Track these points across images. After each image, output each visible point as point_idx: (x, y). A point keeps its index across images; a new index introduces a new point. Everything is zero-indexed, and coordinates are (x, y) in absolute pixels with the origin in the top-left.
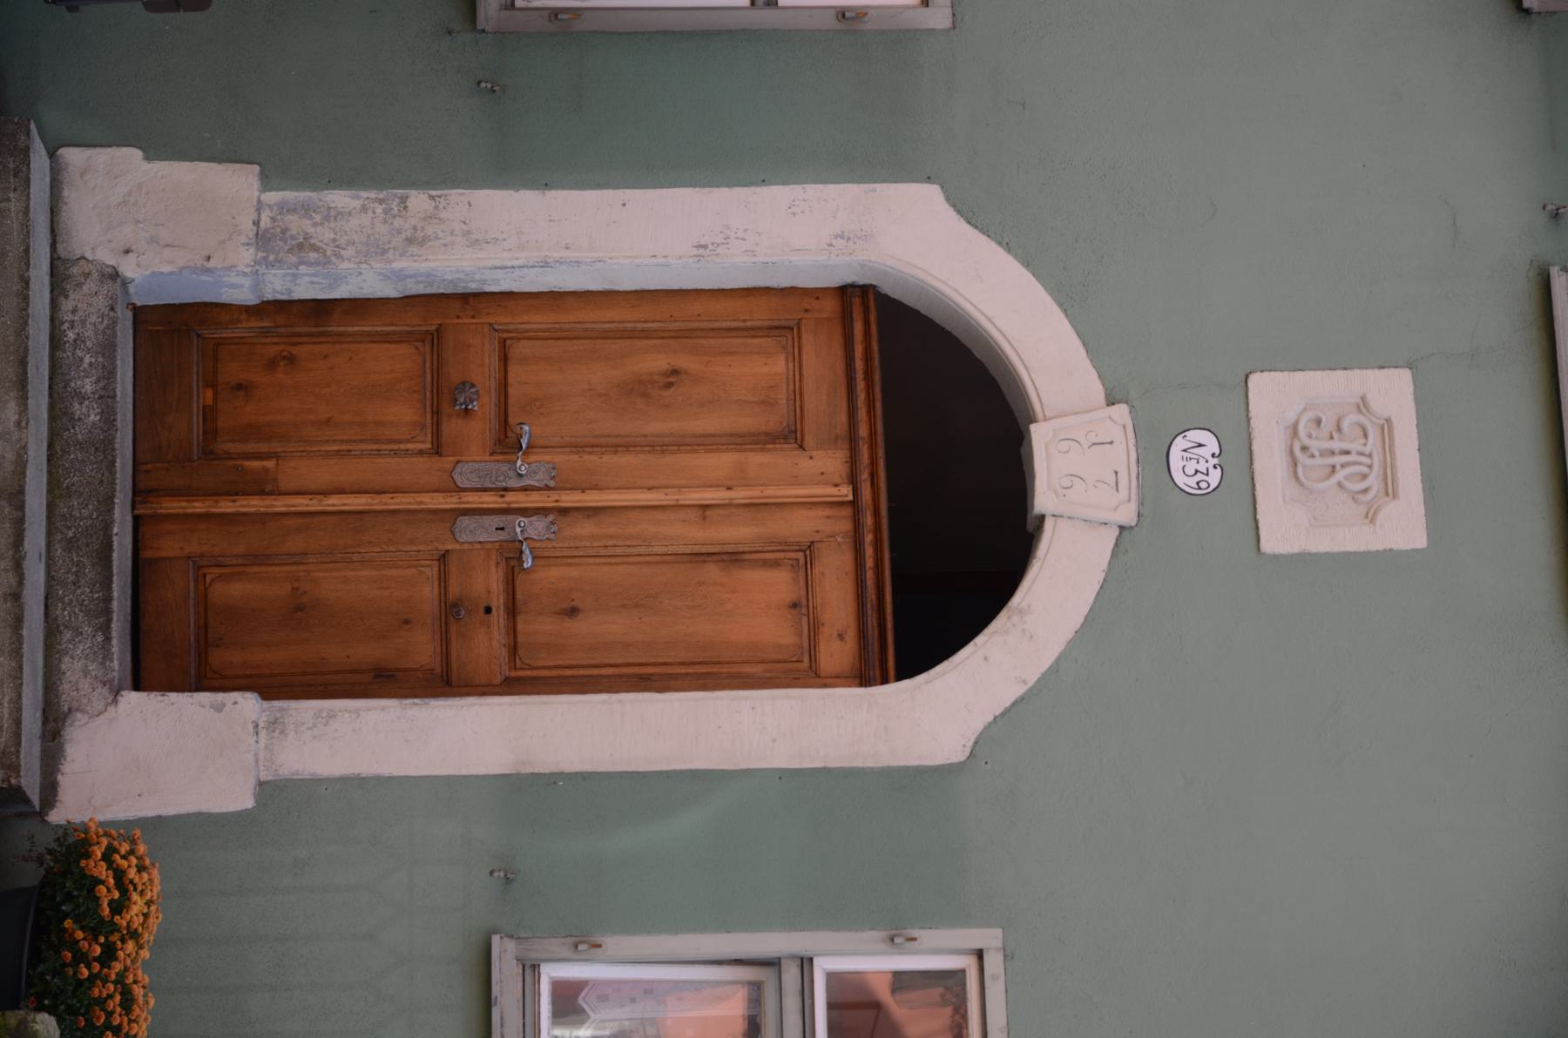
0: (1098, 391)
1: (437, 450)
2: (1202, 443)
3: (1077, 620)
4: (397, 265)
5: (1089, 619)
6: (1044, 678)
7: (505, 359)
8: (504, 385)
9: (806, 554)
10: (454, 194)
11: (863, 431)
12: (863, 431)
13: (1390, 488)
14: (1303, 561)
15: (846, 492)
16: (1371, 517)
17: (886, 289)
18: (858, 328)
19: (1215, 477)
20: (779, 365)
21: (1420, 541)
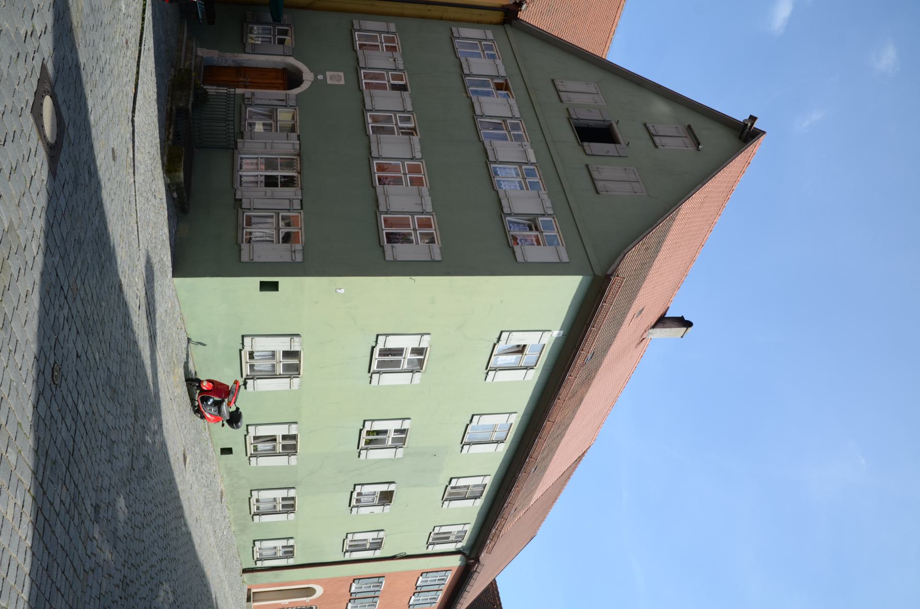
3: (307, 87)
13: (341, 80)
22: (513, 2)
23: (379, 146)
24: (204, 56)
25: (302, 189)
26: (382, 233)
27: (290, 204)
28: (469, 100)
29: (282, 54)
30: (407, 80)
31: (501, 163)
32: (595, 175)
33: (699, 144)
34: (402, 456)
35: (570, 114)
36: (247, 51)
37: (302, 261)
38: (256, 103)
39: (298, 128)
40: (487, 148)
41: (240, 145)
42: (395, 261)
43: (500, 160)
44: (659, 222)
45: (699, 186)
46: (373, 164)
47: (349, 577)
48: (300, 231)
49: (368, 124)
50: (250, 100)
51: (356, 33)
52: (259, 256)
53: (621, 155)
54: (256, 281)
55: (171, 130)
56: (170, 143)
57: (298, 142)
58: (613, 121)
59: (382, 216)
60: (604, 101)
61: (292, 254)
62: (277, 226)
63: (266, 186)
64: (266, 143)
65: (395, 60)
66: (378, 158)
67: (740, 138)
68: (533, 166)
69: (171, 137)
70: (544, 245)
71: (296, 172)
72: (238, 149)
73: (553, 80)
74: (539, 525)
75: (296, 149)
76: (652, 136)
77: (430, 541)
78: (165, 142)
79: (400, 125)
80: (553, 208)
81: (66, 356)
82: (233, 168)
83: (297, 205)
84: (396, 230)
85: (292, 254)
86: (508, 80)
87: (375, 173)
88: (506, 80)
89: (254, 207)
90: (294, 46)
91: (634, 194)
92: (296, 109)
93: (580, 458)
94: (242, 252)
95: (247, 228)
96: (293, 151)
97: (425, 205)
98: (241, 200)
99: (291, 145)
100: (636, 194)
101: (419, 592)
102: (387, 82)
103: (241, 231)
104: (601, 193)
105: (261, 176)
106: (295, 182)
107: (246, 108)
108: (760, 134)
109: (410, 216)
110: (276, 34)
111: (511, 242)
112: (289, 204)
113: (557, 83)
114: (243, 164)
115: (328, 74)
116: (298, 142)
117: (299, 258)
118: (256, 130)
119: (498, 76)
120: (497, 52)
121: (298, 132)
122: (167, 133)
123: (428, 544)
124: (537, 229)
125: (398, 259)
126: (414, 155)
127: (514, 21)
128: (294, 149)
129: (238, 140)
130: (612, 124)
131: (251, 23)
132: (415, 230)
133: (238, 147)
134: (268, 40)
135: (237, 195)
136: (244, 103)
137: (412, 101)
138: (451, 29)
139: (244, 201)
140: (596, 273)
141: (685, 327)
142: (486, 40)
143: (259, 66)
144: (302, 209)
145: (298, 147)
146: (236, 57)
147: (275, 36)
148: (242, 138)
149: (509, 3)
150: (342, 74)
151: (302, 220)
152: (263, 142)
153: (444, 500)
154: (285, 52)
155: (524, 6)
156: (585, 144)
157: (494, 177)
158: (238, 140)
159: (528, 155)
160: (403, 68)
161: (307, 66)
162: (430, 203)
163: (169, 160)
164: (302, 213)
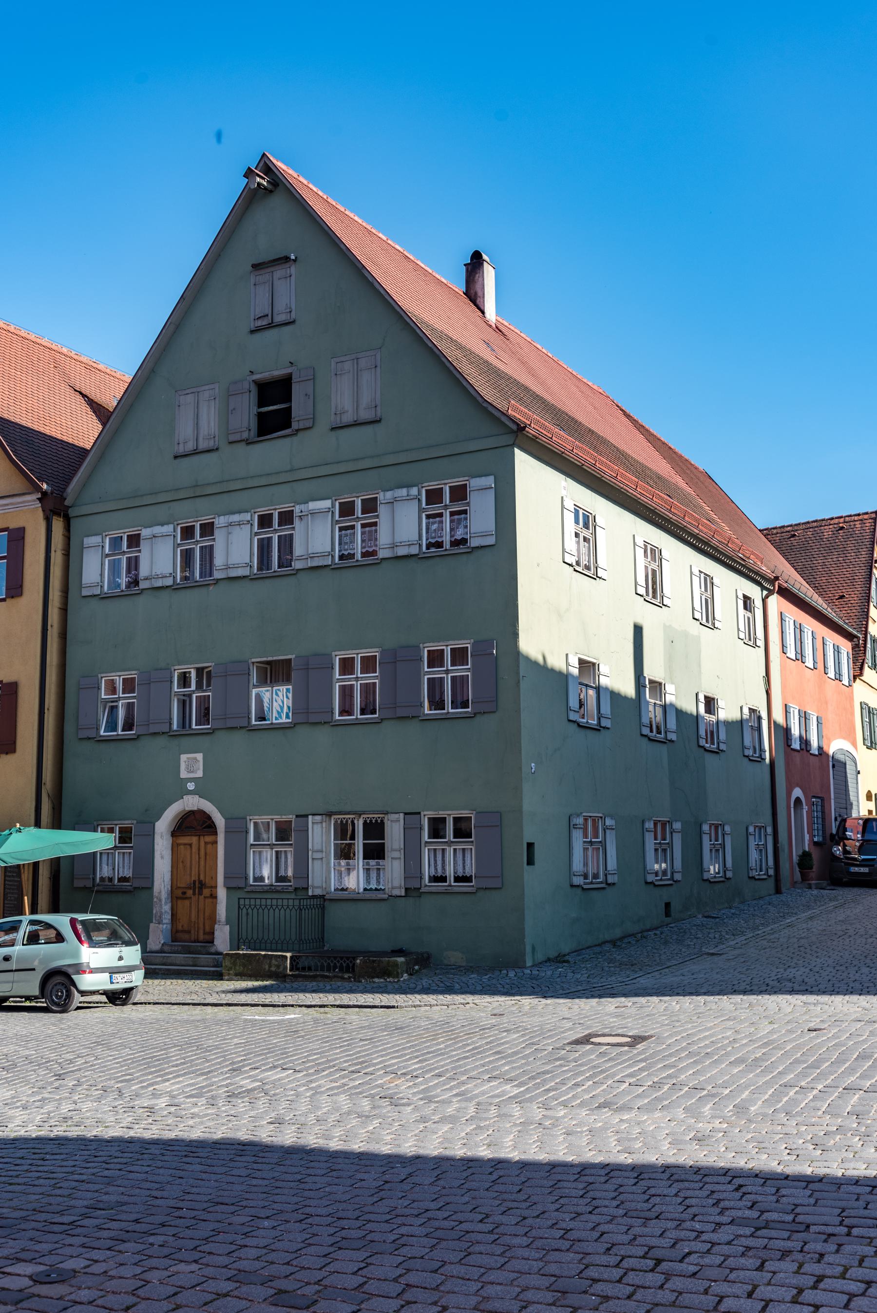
24: (162, 942)
25: (387, 813)
26: (453, 713)
28: (221, 583)
30: (189, 666)
32: (348, 418)
33: (287, 259)
34: (673, 686)
41: (318, 892)
44: (430, 345)
45: (367, 274)
47: (785, 752)
48: (452, 816)
59: (254, 722)
60: (212, 386)
64: (313, 859)
73: (176, 457)
74: (681, 457)
75: (322, 820)
77: (751, 643)
80: (409, 486)
81: (358, 1167)
82: (346, 898)
84: (448, 695)
91: (378, 369)
93: (628, 416)
95: (450, 881)
96: (324, 824)
100: (379, 364)
101: (802, 655)
103: (455, 888)
104: (379, 414)
106: (374, 821)
111: (462, 549)
113: (181, 450)
114: (340, 888)
115: (184, 774)
118: (131, 875)
120: (125, 533)
123: (755, 646)
128: (322, 823)
129: (310, 893)
131: (246, 878)
141: (482, 264)
142: (103, 547)
145: (318, 818)
148: (307, 889)
150: (184, 757)
151: (437, 813)
152: (313, 863)
153: (714, 627)
156: (295, 425)
158: (310, 893)
164: (426, 813)
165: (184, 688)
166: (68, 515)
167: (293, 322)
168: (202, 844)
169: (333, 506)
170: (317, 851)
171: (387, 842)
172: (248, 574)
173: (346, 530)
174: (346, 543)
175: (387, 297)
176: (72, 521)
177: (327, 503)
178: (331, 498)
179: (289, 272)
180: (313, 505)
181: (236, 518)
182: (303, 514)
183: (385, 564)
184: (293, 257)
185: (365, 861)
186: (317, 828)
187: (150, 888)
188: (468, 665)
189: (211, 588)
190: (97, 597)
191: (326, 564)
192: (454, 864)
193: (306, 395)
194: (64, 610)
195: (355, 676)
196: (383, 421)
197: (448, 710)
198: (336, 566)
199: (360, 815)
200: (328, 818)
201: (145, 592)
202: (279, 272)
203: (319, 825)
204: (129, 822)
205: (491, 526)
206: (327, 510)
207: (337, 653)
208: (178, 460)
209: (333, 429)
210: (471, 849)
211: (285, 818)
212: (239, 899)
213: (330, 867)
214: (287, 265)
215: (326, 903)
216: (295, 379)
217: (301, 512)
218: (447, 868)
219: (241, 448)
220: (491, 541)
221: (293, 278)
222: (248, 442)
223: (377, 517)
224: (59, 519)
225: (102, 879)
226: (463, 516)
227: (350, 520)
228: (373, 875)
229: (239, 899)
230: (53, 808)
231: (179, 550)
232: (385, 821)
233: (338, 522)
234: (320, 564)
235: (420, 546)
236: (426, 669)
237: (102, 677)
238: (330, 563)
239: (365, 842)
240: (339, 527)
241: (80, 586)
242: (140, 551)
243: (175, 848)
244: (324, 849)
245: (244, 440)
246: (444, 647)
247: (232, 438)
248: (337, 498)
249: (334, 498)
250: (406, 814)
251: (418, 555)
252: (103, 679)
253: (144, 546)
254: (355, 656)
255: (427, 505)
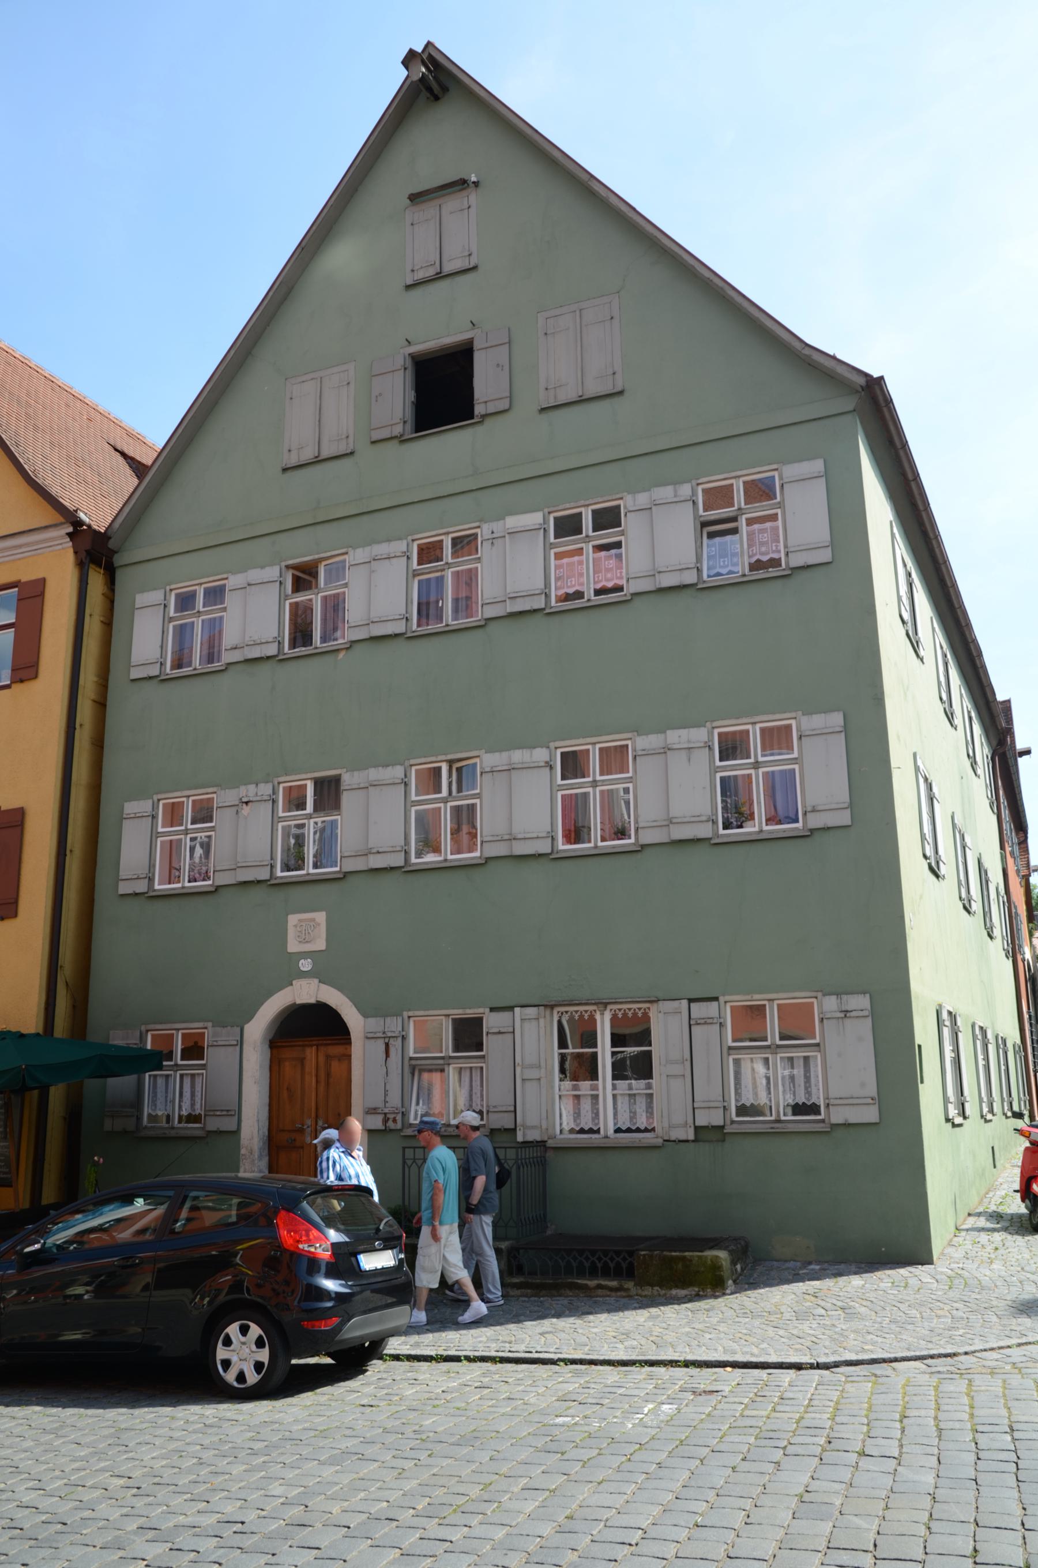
0: (290, 988)
1: (302, 1147)
2: (924, 660)
3: (339, 993)
4: (256, 1157)
5: (339, 990)
6: (351, 1001)
7: (283, 1131)
8: (289, 1131)
9: (328, 1057)
10: (242, 1142)
11: (301, 1043)
12: (301, 1043)
13: (313, 920)
14: (327, 940)
15: (314, 1048)
16: (319, 924)
17: (271, 1036)
18: (279, 1044)
19: (309, 960)
20: (287, 1064)
21: (324, 914)
22: (68, 539)
23: (520, 836)
27: (705, 1023)
28: (357, 648)
29: (238, 1048)
31: (547, 584)
35: (392, 438)
36: (234, 1128)
37: (868, 996)
38: (400, 1105)
39: (468, 1011)
40: (509, 610)
41: (533, 1136)
42: (851, 806)
43: (541, 585)
46: (282, 878)
49: (183, 887)
50: (391, 1116)
51: (157, 887)
52: (863, 1085)
53: (507, 340)
54: (920, 1086)
55: (592, 1283)
56: (629, 1285)
57: (517, 1010)
58: (402, 351)
59: (279, 874)
61: (850, 1017)
62: (768, 1050)
63: (650, 1077)
65: (247, 803)
66: (553, 838)
67: (437, 98)
68: (549, 520)
69: (614, 1284)
70: (346, 585)
71: (602, 1014)
72: (546, 1139)
73: (285, 470)
76: (440, 276)
78: (630, 1297)
79: (445, 792)
80: (676, 483)
83: (710, 1009)
84: (759, 803)
85: (850, 1017)
86: (290, 562)
87: (446, 860)
88: (288, 567)
89: (721, 1098)
90: (210, 1024)
92: (409, 1017)
94: (852, 1121)
96: (542, 1021)
97: (689, 741)
98: (697, 1129)
99: (526, 1025)
102: (312, 821)
103: (789, 1125)
105: (614, 1087)
107: (411, 1124)
108: (434, 54)
109: (159, 839)
110: (172, 1063)
112: (706, 1027)
113: (293, 461)
115: (293, 946)
116: (517, 1010)
117: (860, 1002)
119: (281, 583)
120: (201, 584)
121: (481, 1010)
122: (600, 1292)
124: (734, 519)
125: (848, 800)
126: (543, 764)
127: (111, 544)
129: (520, 1138)
130: (409, 354)
131: (139, 1119)
132: (756, 765)
133: (539, 1139)
134: (187, 1082)
135: (683, 1137)
136: (400, 1130)
137: (375, 767)
138: (133, 680)
139: (701, 1121)
140: (851, 408)
142: (165, 606)
143: (267, 1100)
144: (716, 999)
145: (532, 1011)
146: (251, 1152)
147: (176, 1065)
148: (514, 1130)
149: (71, 550)
150: (293, 919)
151: (749, 997)
154: (235, 1043)
155: (82, 516)
156: (479, 409)
157: (447, 625)
158: (520, 1138)
159: (524, 526)
160: (270, 786)
161: (270, 994)
162: (683, 732)
163: (684, 1284)
165: (172, 826)
166: (112, 564)
167: (475, 268)
168: (322, 1059)
169: (545, 521)
170: (531, 1066)
171: (657, 1049)
172: (403, 630)
173: (608, 550)
174: (762, 544)
175: (631, 214)
176: (119, 575)
177: (536, 518)
178: (541, 510)
179: (466, 203)
180: (513, 522)
181: (382, 549)
182: (495, 535)
183: (638, 602)
184: (474, 179)
185: (622, 1084)
186: (530, 1028)
187: (236, 1133)
188: (628, 772)
189: (341, 655)
190: (155, 681)
191: (536, 607)
192: (736, 1084)
193: (498, 365)
194: (101, 704)
195: (183, 828)
196: (626, 394)
197: (446, 854)
198: (705, 585)
199: (606, 1005)
200: (548, 1012)
201: (232, 668)
202: (451, 204)
203: (534, 1023)
204: (201, 1025)
205: (823, 535)
206: (537, 527)
207: (558, 744)
208: (289, 474)
209: (543, 410)
210: (482, 1068)
211: (470, 1012)
212: (404, 1148)
213: (553, 1094)
214: (464, 193)
215: (550, 1154)
216: (477, 345)
217: (493, 533)
218: (814, 1090)
219: (393, 447)
220: (825, 556)
221: (473, 210)
222: (402, 440)
223: (622, 533)
224: (98, 569)
225: (153, 1118)
226: (576, 558)
227: (574, 542)
228: (586, 1105)
229: (404, 1148)
230: (74, 1007)
231: (287, 603)
232: (652, 1014)
233: (552, 546)
234: (527, 608)
235: (547, 596)
236: (559, 782)
237: (159, 800)
238: (543, 606)
239: (594, 1050)
240: (555, 554)
241: (129, 666)
242: (224, 609)
243: (275, 1066)
244: (543, 1064)
245: (396, 437)
246: (749, 727)
247: (376, 436)
248: (551, 509)
249: (546, 510)
250: (691, 1001)
251: (696, 584)
252: (161, 803)
253: (231, 600)
254: (590, 747)
255: (556, 537)
